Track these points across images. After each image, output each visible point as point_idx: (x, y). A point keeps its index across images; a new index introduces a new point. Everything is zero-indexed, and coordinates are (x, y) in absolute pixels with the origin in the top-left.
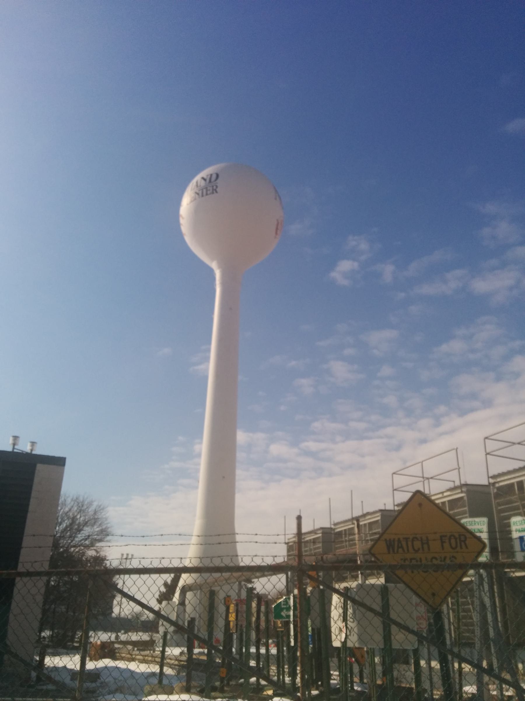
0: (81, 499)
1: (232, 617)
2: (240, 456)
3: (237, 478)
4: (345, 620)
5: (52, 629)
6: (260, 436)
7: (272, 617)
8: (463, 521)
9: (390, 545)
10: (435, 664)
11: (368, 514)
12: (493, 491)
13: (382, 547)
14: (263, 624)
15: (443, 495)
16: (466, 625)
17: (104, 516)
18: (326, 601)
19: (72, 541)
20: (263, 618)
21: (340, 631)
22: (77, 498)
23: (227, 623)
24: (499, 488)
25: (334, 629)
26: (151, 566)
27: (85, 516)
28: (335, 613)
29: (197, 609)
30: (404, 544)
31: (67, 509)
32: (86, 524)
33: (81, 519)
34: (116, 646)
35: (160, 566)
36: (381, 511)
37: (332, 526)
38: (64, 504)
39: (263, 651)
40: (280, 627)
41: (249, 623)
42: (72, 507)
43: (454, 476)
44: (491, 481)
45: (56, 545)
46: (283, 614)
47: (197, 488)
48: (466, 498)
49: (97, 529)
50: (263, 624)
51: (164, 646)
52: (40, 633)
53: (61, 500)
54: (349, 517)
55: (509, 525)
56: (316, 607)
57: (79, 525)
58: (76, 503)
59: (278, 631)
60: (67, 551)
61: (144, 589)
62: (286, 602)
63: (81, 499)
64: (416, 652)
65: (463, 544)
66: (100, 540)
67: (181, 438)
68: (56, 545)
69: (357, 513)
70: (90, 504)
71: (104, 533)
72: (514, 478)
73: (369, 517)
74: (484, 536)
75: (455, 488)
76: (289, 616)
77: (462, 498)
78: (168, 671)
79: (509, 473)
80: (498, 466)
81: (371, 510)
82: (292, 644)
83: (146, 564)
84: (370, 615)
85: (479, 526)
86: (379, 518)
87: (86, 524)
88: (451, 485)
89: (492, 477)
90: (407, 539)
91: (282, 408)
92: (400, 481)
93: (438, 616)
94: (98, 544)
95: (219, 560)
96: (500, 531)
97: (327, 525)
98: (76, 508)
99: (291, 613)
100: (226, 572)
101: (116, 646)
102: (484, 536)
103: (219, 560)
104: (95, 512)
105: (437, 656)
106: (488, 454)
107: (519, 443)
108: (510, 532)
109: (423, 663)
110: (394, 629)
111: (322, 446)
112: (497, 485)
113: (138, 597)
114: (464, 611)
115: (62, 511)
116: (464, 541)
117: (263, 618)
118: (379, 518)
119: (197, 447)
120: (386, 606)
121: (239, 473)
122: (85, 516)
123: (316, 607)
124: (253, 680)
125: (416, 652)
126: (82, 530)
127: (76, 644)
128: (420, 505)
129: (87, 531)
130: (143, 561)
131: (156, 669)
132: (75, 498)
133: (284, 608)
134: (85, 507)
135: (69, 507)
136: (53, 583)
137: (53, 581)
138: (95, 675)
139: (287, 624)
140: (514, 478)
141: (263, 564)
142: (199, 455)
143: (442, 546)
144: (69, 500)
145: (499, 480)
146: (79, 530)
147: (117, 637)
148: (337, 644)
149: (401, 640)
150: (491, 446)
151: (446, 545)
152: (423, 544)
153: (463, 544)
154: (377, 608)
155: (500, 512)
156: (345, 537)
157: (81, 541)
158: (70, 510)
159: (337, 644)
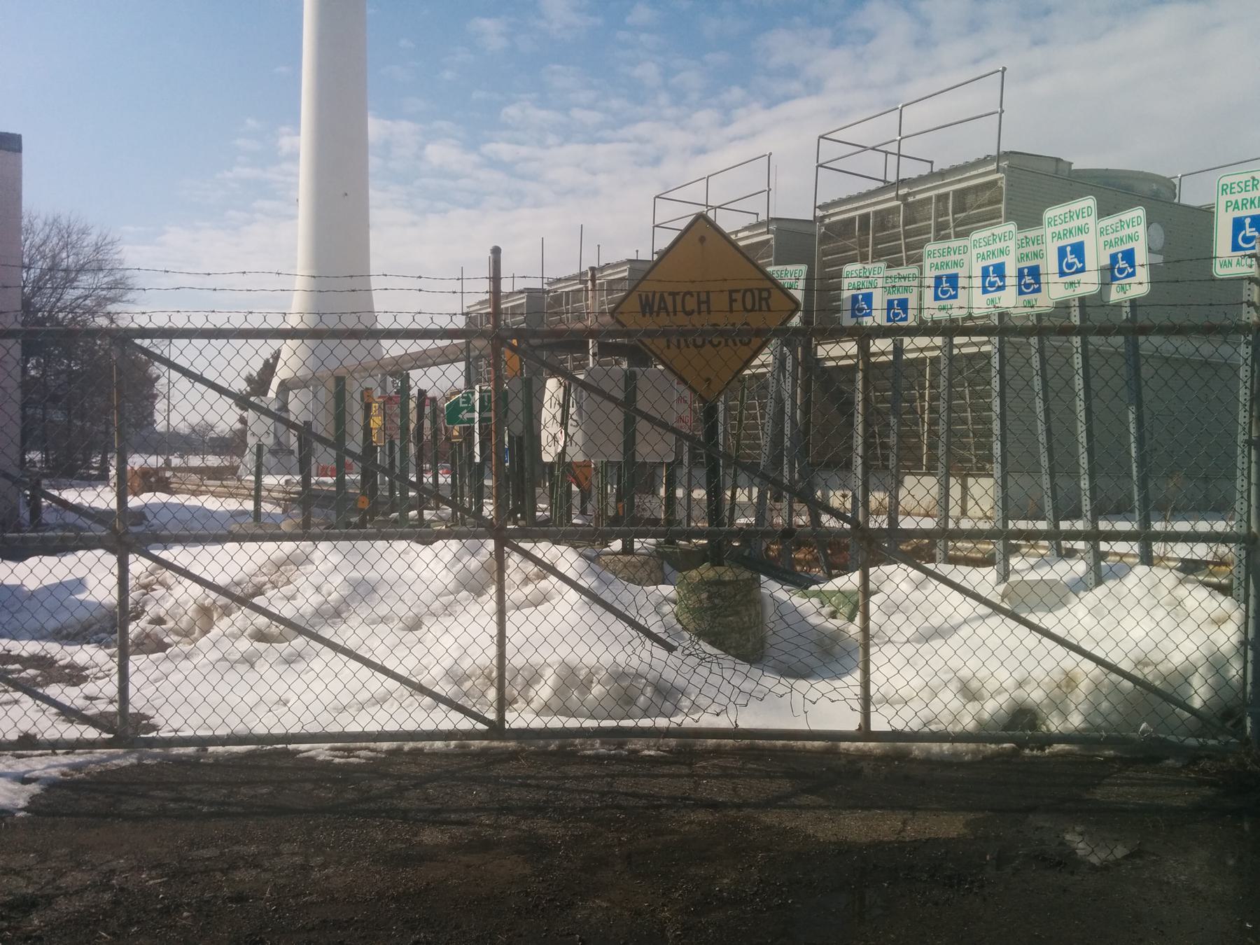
0: (64, 223)
1: (376, 422)
2: (374, 162)
3: (371, 203)
4: (564, 424)
5: (45, 450)
6: (405, 127)
7: (442, 423)
8: (769, 269)
9: (647, 307)
10: (699, 494)
11: (608, 266)
12: (820, 230)
13: (634, 304)
14: (427, 433)
15: (621, 746)
16: (749, 437)
17: (116, 257)
18: (534, 389)
19: (58, 300)
20: (427, 424)
21: (553, 439)
22: (55, 220)
23: (367, 431)
24: (828, 227)
25: (545, 437)
26: (227, 326)
27: (77, 254)
28: (549, 412)
29: (311, 407)
30: (669, 300)
31: (38, 241)
32: (81, 269)
33: (68, 260)
34: (168, 474)
35: (246, 326)
36: (630, 261)
37: (546, 287)
38: (31, 231)
39: (428, 479)
40: (456, 437)
41: (405, 428)
42: (48, 237)
43: (758, 205)
44: (819, 213)
45: (27, 304)
46: (465, 415)
47: (294, 217)
48: (773, 242)
49: (106, 280)
50: (427, 433)
51: (258, 475)
52: (23, 454)
53: (25, 222)
54: (576, 271)
55: (839, 275)
56: (516, 406)
57: (67, 270)
58: (55, 231)
59: (453, 444)
60: (51, 318)
61: (220, 363)
62: (468, 400)
63: (64, 223)
64: (672, 467)
65: (764, 303)
66: (113, 300)
67: (251, 123)
68: (27, 304)
69: (590, 261)
70: (84, 232)
71: (120, 287)
72: (856, 209)
73: (610, 271)
74: (799, 295)
75: (759, 225)
76: (472, 420)
77: (768, 241)
78: (267, 507)
79: (850, 199)
80: (835, 188)
81: (613, 261)
82: (477, 459)
83: (219, 321)
84: (609, 406)
85: (793, 276)
86: (626, 274)
87: (81, 269)
88: (752, 220)
89: (819, 207)
90: (674, 294)
91: (448, 75)
92: (667, 211)
93: (710, 412)
94: (111, 308)
95: (354, 319)
96: (824, 287)
97: (536, 284)
98: (55, 240)
99: (476, 415)
100: (367, 338)
101: (168, 474)
102: (799, 295)
103: (354, 319)
104: (97, 249)
105: (704, 481)
106: (821, 166)
107: (873, 149)
108: (839, 288)
109: (680, 493)
110: (642, 425)
111: (524, 151)
112: (827, 221)
113: (210, 375)
114: (749, 437)
115: (28, 243)
116: (766, 300)
117: (427, 424)
118: (626, 274)
119: (285, 143)
120: (629, 424)
121: (375, 195)
122: (77, 254)
123: (516, 406)
124: (413, 513)
125: (672, 467)
126: (74, 280)
127: (93, 472)
128: (702, 239)
129: (86, 280)
130: (212, 317)
131: (249, 505)
132: (51, 220)
133: (463, 409)
134: (74, 237)
135: (41, 236)
136: (33, 373)
137: (34, 368)
138: (140, 515)
139: (469, 432)
140: (856, 209)
141: (433, 327)
142: (294, 157)
143: (731, 305)
144: (39, 224)
145: (831, 211)
146: (69, 282)
147: (168, 462)
148: (547, 458)
149: (654, 448)
150: (829, 151)
151: (738, 306)
152: (699, 303)
153: (764, 303)
154: (620, 395)
155: (825, 265)
156: (567, 304)
157: (78, 298)
158: (44, 243)
159: (547, 458)
